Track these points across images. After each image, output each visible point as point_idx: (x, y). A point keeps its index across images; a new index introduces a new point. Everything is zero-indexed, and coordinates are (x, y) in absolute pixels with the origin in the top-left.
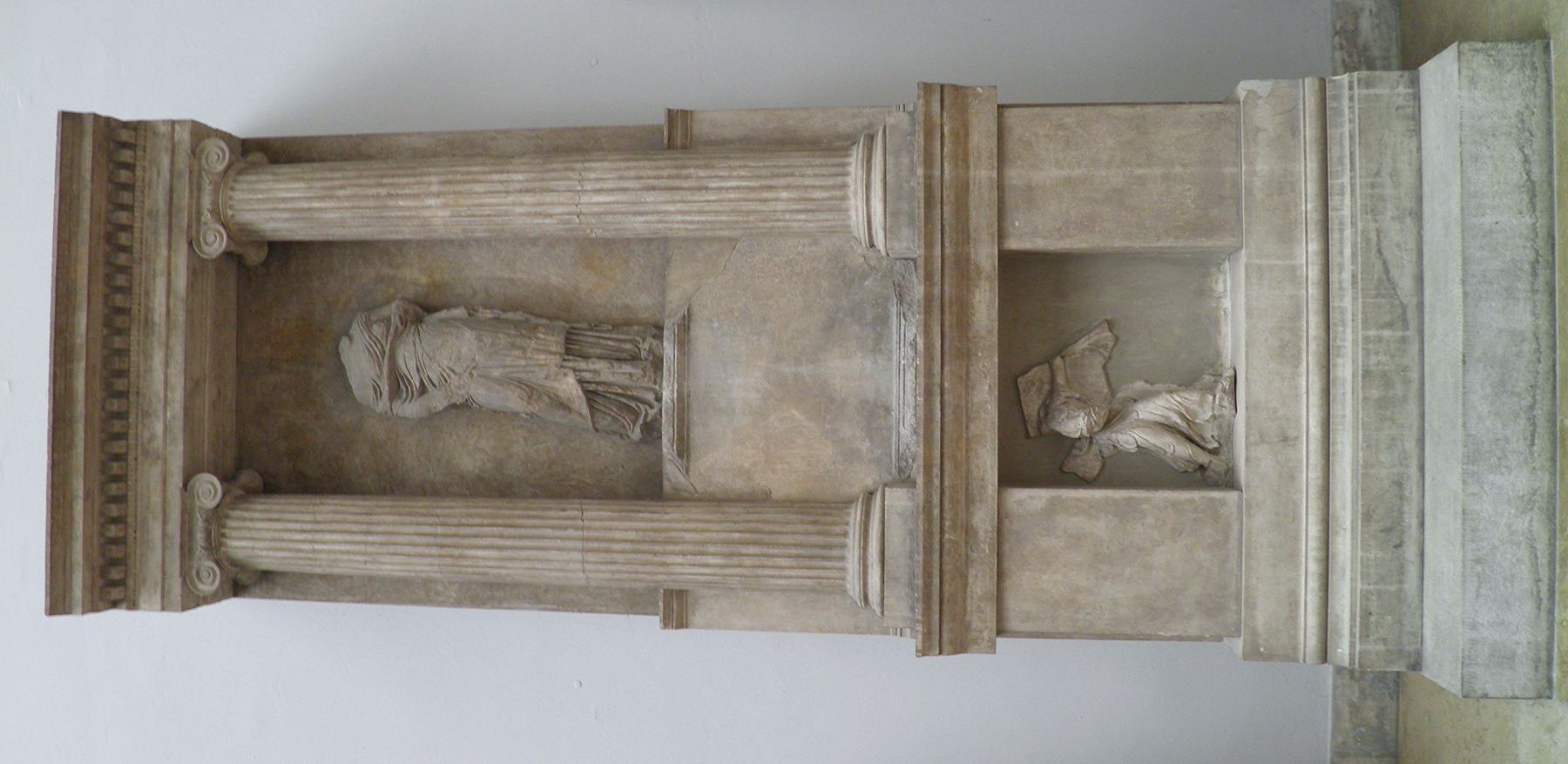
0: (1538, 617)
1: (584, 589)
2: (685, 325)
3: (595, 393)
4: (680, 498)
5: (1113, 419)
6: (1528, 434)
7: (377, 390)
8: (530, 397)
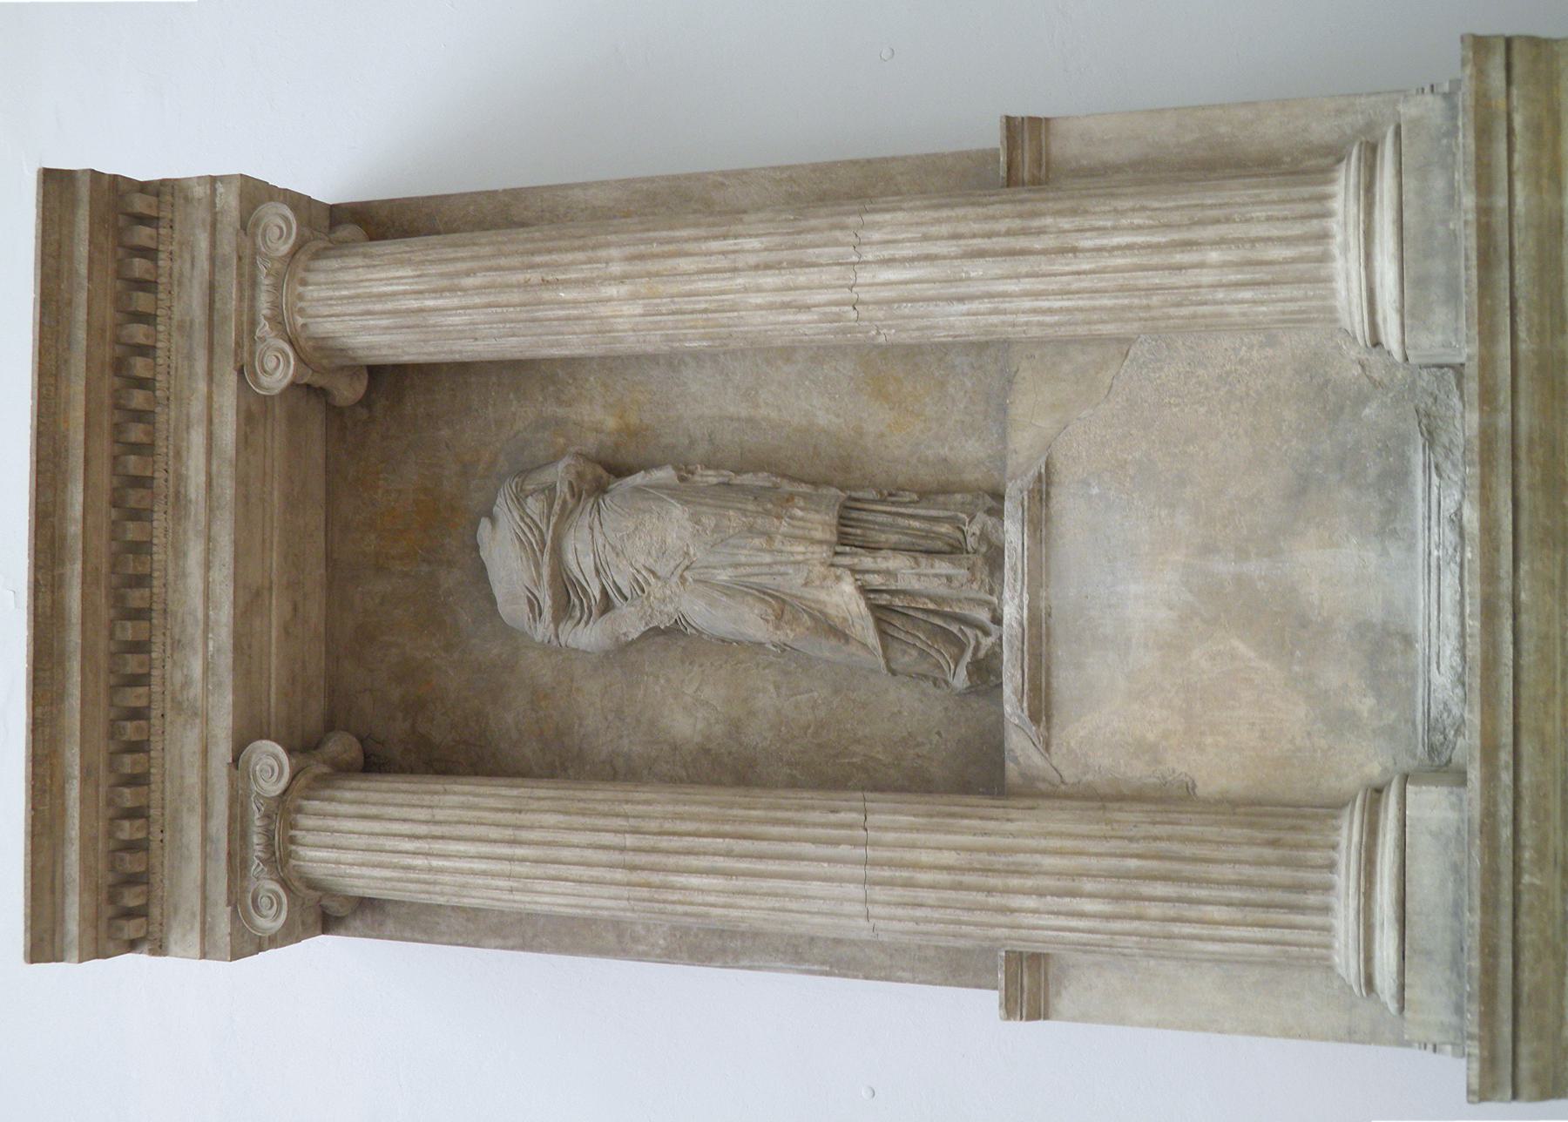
2: (1042, 491)
3: (888, 609)
4: (1033, 792)
7: (534, 604)
8: (779, 617)
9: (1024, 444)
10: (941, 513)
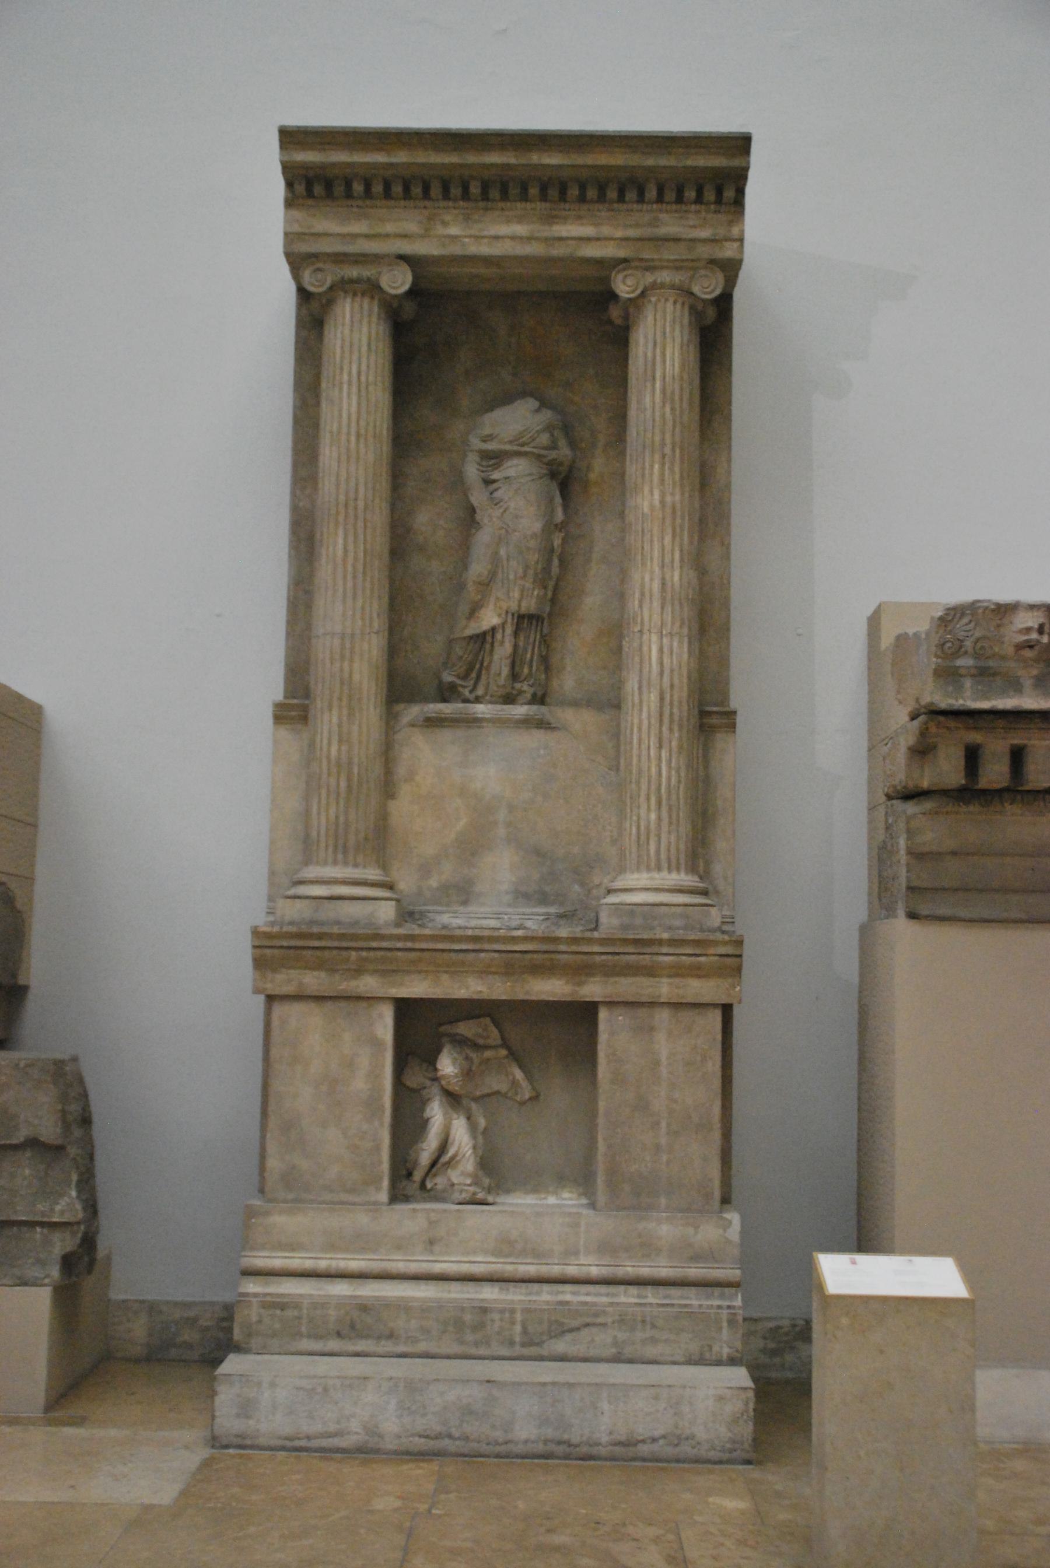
0: (280, 1438)
1: (309, 627)
2: (542, 724)
4: (390, 717)
5: (453, 1099)
6: (428, 1432)
8: (480, 583)
9: (567, 715)
10: (534, 668)
